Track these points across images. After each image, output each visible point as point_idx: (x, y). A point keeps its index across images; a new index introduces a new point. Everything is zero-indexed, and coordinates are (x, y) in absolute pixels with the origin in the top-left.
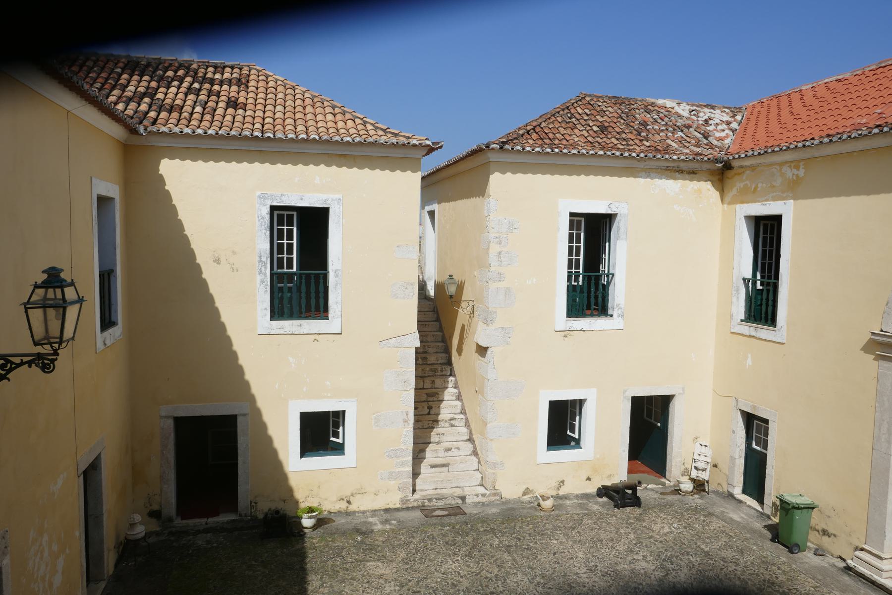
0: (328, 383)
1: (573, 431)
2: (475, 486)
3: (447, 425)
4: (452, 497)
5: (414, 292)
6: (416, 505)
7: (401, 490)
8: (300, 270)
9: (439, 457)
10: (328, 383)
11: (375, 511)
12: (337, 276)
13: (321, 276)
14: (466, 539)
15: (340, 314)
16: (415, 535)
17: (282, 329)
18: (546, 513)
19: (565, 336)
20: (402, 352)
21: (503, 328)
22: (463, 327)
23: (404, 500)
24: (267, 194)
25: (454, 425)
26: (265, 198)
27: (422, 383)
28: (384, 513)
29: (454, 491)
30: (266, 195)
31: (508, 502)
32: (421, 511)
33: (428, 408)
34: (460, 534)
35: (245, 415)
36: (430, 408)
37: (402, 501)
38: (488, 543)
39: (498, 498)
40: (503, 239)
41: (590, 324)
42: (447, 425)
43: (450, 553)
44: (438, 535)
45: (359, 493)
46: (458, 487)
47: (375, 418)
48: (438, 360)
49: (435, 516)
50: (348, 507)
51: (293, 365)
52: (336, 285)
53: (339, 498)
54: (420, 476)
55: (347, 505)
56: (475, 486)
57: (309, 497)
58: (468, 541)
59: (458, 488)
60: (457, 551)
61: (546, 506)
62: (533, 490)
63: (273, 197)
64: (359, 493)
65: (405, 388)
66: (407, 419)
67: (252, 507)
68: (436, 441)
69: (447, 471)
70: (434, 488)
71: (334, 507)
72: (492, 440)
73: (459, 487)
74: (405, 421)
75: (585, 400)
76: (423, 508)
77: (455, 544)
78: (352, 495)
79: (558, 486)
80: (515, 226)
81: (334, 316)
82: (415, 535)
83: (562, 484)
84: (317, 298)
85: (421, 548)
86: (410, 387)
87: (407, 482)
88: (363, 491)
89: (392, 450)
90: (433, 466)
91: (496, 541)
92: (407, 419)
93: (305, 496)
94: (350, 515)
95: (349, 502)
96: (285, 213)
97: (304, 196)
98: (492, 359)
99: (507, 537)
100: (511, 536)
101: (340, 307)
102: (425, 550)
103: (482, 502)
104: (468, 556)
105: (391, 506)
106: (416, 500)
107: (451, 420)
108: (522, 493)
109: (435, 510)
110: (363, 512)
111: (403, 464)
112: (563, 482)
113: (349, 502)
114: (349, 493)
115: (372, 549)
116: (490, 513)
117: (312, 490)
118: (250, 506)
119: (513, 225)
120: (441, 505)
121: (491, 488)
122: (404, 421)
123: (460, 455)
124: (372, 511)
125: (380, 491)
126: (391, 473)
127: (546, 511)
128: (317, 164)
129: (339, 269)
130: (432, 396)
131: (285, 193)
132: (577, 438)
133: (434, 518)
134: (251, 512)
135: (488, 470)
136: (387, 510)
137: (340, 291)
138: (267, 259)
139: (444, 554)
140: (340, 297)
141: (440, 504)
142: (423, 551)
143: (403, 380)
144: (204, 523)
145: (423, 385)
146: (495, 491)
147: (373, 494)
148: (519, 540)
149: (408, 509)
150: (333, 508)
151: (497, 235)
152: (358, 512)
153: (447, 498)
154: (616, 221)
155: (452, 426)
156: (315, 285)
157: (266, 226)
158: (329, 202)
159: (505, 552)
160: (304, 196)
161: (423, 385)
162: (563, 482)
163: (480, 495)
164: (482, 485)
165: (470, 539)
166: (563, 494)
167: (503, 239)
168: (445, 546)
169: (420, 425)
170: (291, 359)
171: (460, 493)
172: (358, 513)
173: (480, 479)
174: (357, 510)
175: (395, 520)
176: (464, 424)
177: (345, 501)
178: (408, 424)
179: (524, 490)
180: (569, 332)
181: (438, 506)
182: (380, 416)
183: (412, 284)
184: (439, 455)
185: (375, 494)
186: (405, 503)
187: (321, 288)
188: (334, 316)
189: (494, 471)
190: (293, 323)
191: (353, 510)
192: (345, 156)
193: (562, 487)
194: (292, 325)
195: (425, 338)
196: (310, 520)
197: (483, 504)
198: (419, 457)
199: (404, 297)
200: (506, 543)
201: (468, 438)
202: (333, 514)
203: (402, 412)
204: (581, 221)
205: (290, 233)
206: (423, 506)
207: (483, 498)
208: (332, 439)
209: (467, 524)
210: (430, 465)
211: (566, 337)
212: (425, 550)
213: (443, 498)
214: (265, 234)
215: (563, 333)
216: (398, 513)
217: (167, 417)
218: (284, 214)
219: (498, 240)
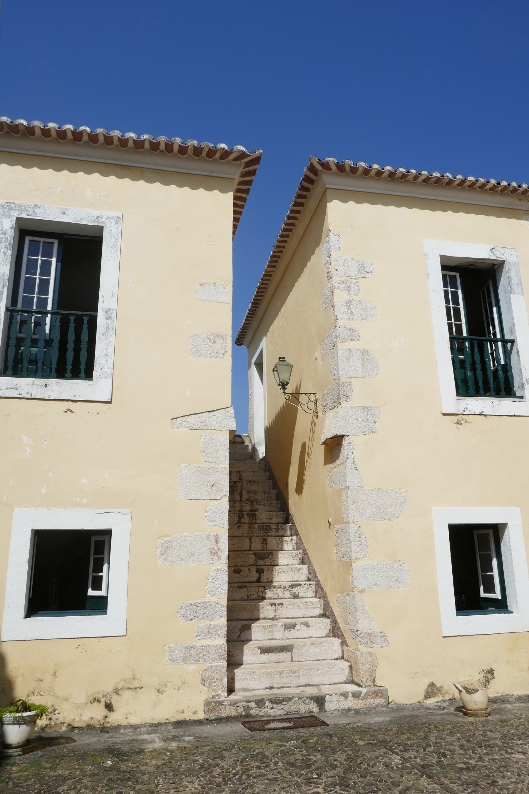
0: (85, 481)
1: (490, 588)
2: (340, 683)
3: (287, 594)
4: (299, 699)
5: (227, 349)
6: (233, 713)
7: (207, 684)
9: (276, 639)
10: (85, 481)
11: (158, 724)
12: (108, 318)
13: (86, 319)
14: (331, 758)
15: (110, 372)
16: (226, 754)
17: (14, 390)
18: (478, 719)
19: (459, 423)
20: (208, 437)
21: (364, 407)
22: (304, 445)
23: (211, 702)
24: (14, 203)
25: (298, 595)
26: (10, 209)
27: (248, 543)
28: (174, 728)
29: (303, 690)
30: (12, 205)
31: (400, 708)
32: (243, 723)
33: (257, 571)
34: (319, 751)
36: (260, 571)
37: (208, 704)
38: (379, 762)
39: (381, 701)
40: (352, 285)
41: (493, 407)
42: (287, 594)
43: (299, 780)
44: (274, 754)
45: (129, 688)
46: (308, 685)
47: (162, 546)
48: (271, 519)
49: (269, 729)
50: (106, 717)
51: (28, 449)
52: (107, 330)
53: (92, 698)
54: (242, 667)
55: (105, 712)
56: (340, 683)
57: (33, 693)
58: (336, 760)
59: (311, 687)
60: (315, 776)
61: (475, 703)
62: (441, 687)
63: (23, 208)
64: (129, 688)
65: (213, 495)
66: (215, 548)
68: (271, 617)
69: (290, 660)
70: (268, 686)
71: (81, 715)
72: (362, 591)
73: (313, 686)
74: (214, 553)
75: (505, 525)
76: (247, 720)
77: (309, 766)
78: (116, 692)
79: (484, 680)
80: (367, 269)
81: (100, 375)
82: (226, 754)
83: (490, 676)
84: (77, 351)
85: (235, 774)
86: (222, 495)
87: (217, 667)
88: (137, 684)
89: (191, 604)
90: (265, 650)
91: (396, 760)
92: (215, 548)
93: (26, 693)
94: (108, 732)
95: (109, 707)
96: (42, 240)
97: (67, 210)
98: (351, 454)
99: (417, 752)
100: (424, 750)
101: (111, 362)
102: (244, 777)
103: (354, 709)
104: (340, 784)
105: (188, 716)
106: (234, 703)
107: (292, 586)
108: (423, 693)
109: (269, 722)
110: (134, 727)
111: (210, 632)
112: (491, 672)
113: (109, 707)
114: (109, 688)
115: (129, 779)
116: (372, 722)
117: (41, 681)
119: (364, 268)
120: (280, 715)
121: (368, 683)
122: (211, 553)
123: (310, 635)
124: (152, 725)
125: (168, 684)
126: (188, 649)
127: (476, 715)
128: (88, 172)
129: (112, 308)
130: (264, 559)
131: (39, 204)
132: (500, 598)
133: (267, 732)
135: (360, 647)
136: (179, 724)
137: (112, 339)
138: (3, 288)
139: (287, 782)
140: (111, 349)
141: (278, 711)
142: (239, 779)
143: (209, 482)
146: (376, 689)
147: (155, 691)
148: (444, 755)
149: (219, 720)
150: (77, 718)
151: (343, 279)
152: (125, 727)
154: (504, 269)
155: (296, 596)
157: (7, 244)
158: (103, 220)
159: (421, 776)
160: (67, 210)
162: (491, 672)
163: (350, 695)
164: (352, 682)
165: (341, 757)
166: (496, 695)
167: (352, 285)
168: (287, 769)
169: (238, 578)
170: (25, 439)
171: (314, 692)
172: (125, 729)
173: (347, 671)
174: (124, 723)
175: (191, 736)
176: (313, 594)
177: (102, 705)
178: (219, 558)
179: (426, 687)
180: (464, 417)
181: (274, 716)
182: (171, 541)
183: (222, 337)
184: (275, 637)
185: (158, 690)
187: (85, 337)
188: (100, 375)
189: (371, 650)
190: (34, 381)
191: (116, 724)
192: (129, 167)
193: (492, 682)
194: (33, 385)
195: (253, 495)
196: (17, 726)
197: (357, 712)
198: (242, 637)
200: (418, 760)
201: (322, 612)
202: (76, 731)
203: (208, 536)
204: (455, 277)
205: (46, 267)
206: (248, 716)
207: (355, 701)
208: (91, 592)
209: (331, 736)
210: (259, 648)
211: (460, 424)
212: (244, 777)
213: (284, 701)
214: (5, 253)
215: (455, 418)
216: (199, 728)
219: (344, 285)
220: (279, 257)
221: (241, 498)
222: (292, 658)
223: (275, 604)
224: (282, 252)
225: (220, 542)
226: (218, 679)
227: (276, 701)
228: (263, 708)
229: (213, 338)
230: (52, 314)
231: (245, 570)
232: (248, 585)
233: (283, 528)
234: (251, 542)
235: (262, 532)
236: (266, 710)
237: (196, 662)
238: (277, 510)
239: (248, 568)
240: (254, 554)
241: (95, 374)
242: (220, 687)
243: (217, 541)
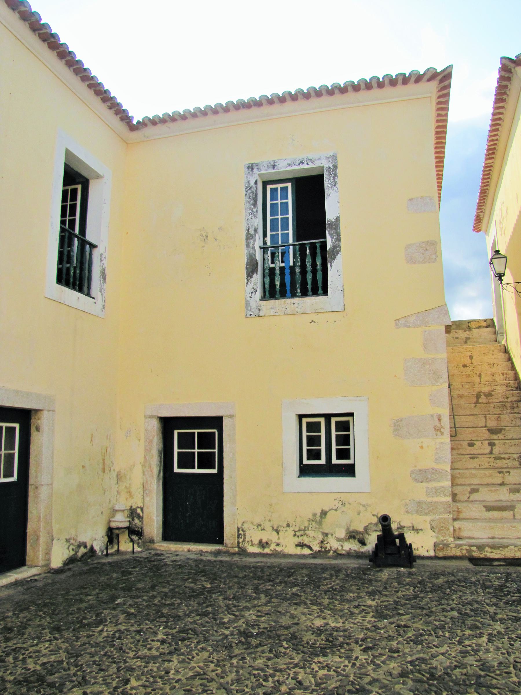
7: (436, 530)
8: (297, 241)
35: (231, 416)
37: (435, 545)
48: (507, 398)
67: (239, 536)
68: (499, 483)
69: (512, 517)
70: (490, 536)
92: (439, 425)
106: (458, 546)
118: (237, 533)
122: (435, 429)
134: (239, 543)
144: (186, 550)
145: (486, 422)
149: (445, 558)
153: (507, 546)
156: (317, 280)
161: (486, 422)
178: (442, 434)
186: (442, 549)
199: (423, 260)
217: (152, 417)
218: (199, 468)
220: (494, 149)
221: (480, 380)
222: (514, 516)
223: (502, 472)
224: (496, 144)
225: (442, 421)
226: (445, 528)
227: (493, 547)
228: (483, 551)
229: (424, 245)
230: (293, 245)
231: (478, 443)
232: (480, 456)
233: (518, 406)
234: (486, 420)
235: (498, 410)
236: (486, 553)
237: (426, 514)
238: (515, 389)
239: (480, 442)
240: (488, 430)
241: (329, 290)
242: (447, 534)
243: (440, 420)
